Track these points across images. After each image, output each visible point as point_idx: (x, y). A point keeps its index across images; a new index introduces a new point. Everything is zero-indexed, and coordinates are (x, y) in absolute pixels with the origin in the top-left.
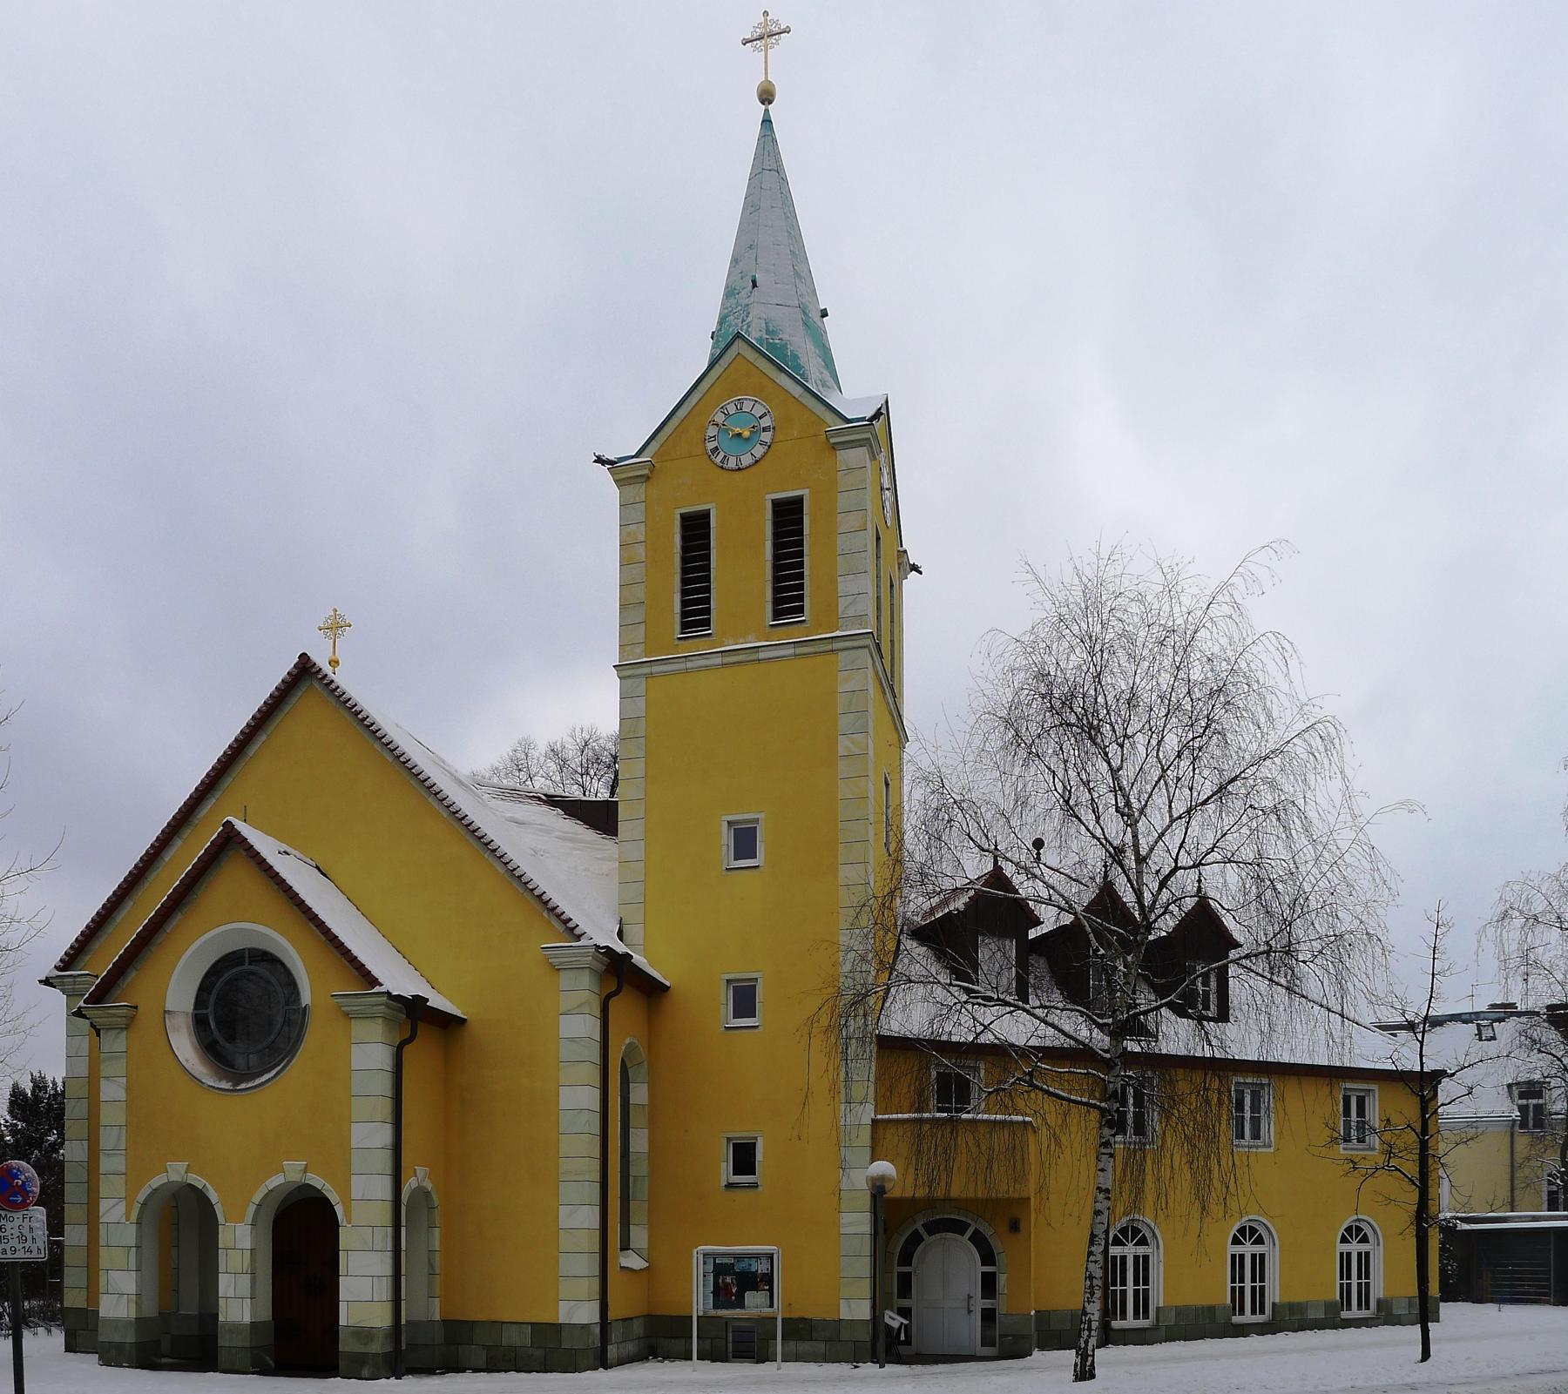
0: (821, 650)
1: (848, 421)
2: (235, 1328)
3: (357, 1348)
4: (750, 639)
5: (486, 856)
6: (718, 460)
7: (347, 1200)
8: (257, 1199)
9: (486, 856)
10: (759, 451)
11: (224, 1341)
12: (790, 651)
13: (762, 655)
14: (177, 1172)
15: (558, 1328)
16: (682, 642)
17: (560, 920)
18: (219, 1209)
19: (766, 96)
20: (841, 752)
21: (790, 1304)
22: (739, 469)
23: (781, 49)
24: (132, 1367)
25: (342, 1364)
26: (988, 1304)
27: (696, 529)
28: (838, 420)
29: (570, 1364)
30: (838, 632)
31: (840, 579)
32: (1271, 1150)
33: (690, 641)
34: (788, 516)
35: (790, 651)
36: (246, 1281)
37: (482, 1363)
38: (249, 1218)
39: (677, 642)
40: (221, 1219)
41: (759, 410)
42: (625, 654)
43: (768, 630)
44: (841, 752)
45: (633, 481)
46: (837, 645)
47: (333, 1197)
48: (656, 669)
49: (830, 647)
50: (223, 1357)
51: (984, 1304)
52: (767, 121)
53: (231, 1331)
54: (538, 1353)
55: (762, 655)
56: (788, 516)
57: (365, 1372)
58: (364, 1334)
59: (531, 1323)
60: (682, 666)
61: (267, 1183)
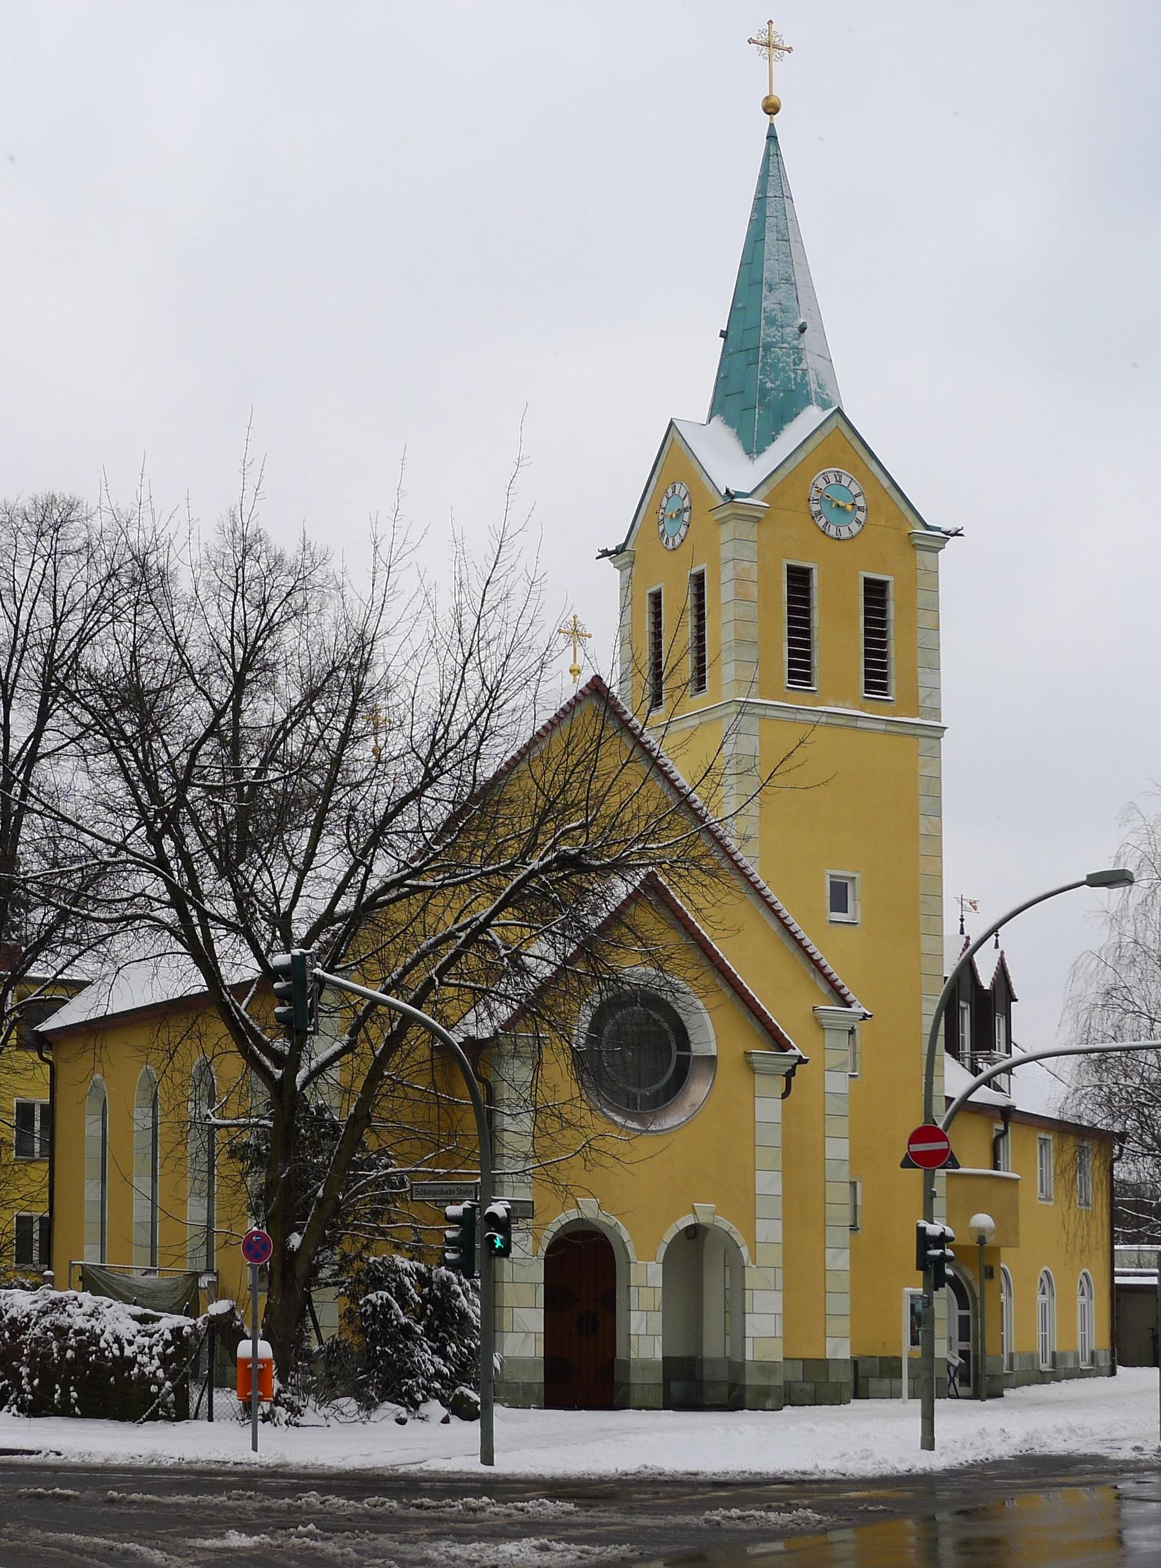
0: (907, 732)
1: (928, 527)
2: (647, 1365)
3: (761, 1381)
4: (848, 705)
5: (760, 911)
6: (821, 523)
7: (753, 1244)
8: (668, 1237)
9: (760, 911)
10: (855, 528)
11: (636, 1378)
12: (882, 727)
13: (860, 724)
14: (589, 1209)
15: (825, 1362)
16: (789, 691)
17: (828, 980)
18: (630, 1248)
19: (771, 108)
20: (922, 831)
21: (884, 1344)
22: (838, 539)
23: (784, 65)
24: (541, 1408)
25: (749, 1396)
26: (964, 1346)
27: (799, 579)
28: (921, 526)
29: (835, 1398)
30: (918, 718)
31: (920, 670)
32: (1051, 1203)
33: (797, 692)
34: (875, 592)
35: (882, 727)
36: (658, 1318)
37: (661, 1406)
38: (661, 1256)
39: (786, 691)
40: (633, 1257)
41: (855, 489)
42: (741, 690)
43: (862, 701)
44: (922, 831)
45: (747, 518)
46: (919, 731)
47: (739, 1239)
48: (769, 712)
49: (913, 732)
50: (636, 1396)
51: (962, 1346)
52: (772, 137)
53: (643, 1369)
54: (810, 1387)
55: (860, 724)
56: (875, 592)
57: (769, 1404)
58: (767, 1368)
59: (803, 1359)
60: (793, 716)
61: (677, 1222)
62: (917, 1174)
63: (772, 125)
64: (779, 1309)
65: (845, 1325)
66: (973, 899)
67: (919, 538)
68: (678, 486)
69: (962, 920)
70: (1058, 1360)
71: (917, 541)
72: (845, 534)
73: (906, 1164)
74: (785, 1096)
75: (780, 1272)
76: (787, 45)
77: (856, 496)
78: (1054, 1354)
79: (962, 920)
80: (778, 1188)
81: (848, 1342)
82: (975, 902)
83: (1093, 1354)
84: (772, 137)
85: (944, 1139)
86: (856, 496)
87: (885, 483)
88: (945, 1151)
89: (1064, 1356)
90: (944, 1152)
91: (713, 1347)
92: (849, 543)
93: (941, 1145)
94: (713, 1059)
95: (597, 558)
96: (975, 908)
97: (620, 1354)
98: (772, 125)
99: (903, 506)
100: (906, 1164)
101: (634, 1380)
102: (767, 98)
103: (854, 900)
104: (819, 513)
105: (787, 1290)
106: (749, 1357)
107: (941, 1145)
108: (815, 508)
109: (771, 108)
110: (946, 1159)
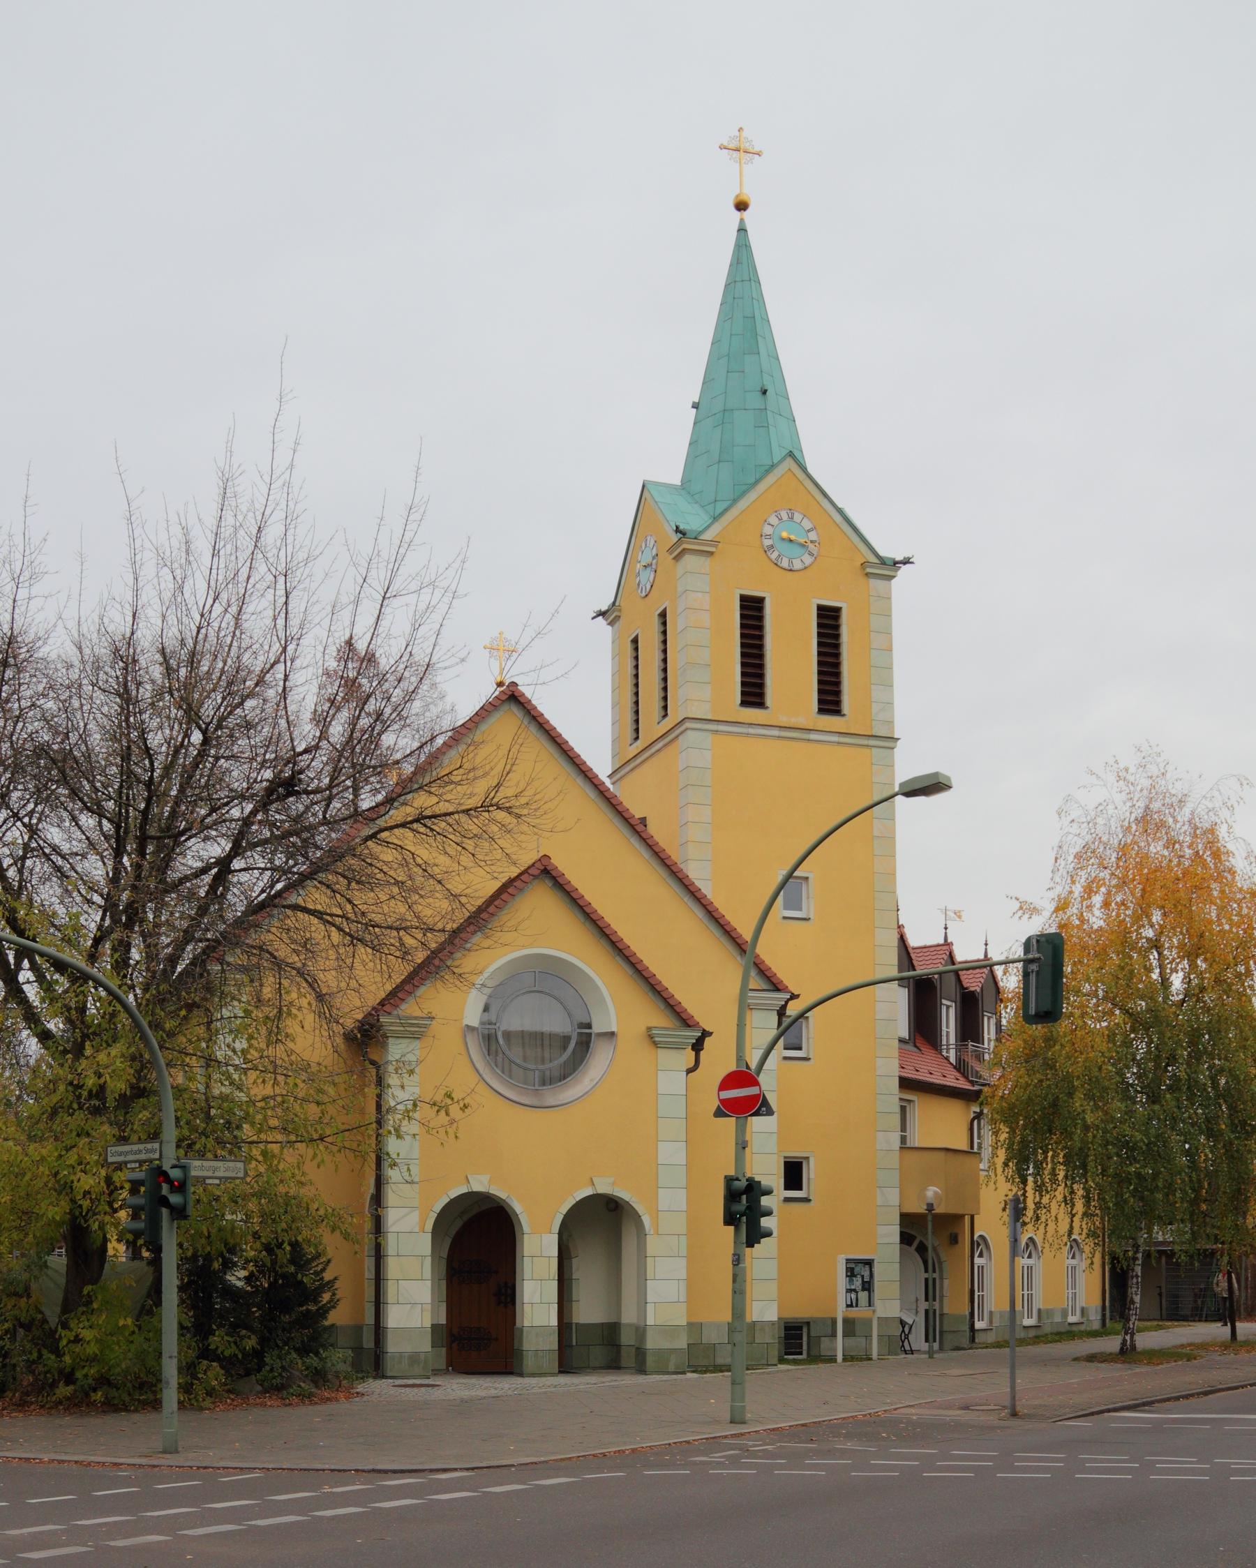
3: (665, 1345)
6: (774, 556)
27: (752, 610)
34: (829, 619)
50: (529, 1363)
52: (742, 230)
56: (829, 619)
62: (730, 1122)
63: (742, 220)
64: (683, 1274)
65: (772, 1289)
66: (957, 908)
67: (870, 567)
68: (648, 538)
69: (946, 928)
70: (1044, 1315)
71: (869, 570)
72: (797, 565)
73: (719, 1113)
74: (689, 1071)
75: (683, 1239)
76: (757, 149)
77: (809, 531)
78: (1039, 1310)
79: (946, 928)
80: (681, 1158)
81: (775, 1306)
82: (960, 912)
83: (1083, 1310)
84: (742, 230)
85: (756, 1083)
86: (809, 531)
87: (838, 518)
88: (756, 1097)
89: (1050, 1313)
90: (755, 1098)
91: (628, 1317)
92: (801, 573)
93: (752, 1091)
94: (612, 1034)
95: (593, 618)
96: (960, 917)
97: (518, 1325)
98: (742, 220)
99: (856, 539)
100: (719, 1113)
101: (526, 1346)
102: (737, 196)
103: (808, 898)
104: (772, 546)
105: (691, 1259)
106: (650, 1321)
107: (752, 1091)
108: (767, 542)
109: (741, 206)
110: (758, 1106)
